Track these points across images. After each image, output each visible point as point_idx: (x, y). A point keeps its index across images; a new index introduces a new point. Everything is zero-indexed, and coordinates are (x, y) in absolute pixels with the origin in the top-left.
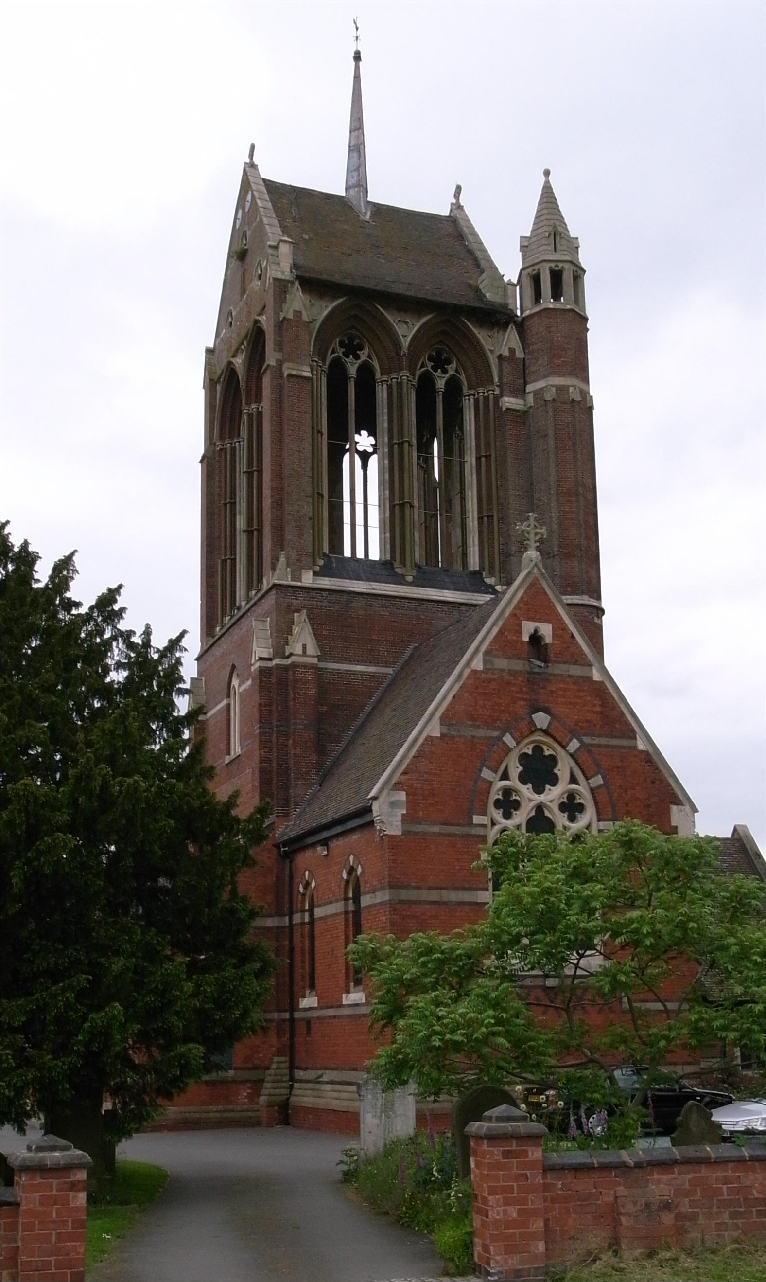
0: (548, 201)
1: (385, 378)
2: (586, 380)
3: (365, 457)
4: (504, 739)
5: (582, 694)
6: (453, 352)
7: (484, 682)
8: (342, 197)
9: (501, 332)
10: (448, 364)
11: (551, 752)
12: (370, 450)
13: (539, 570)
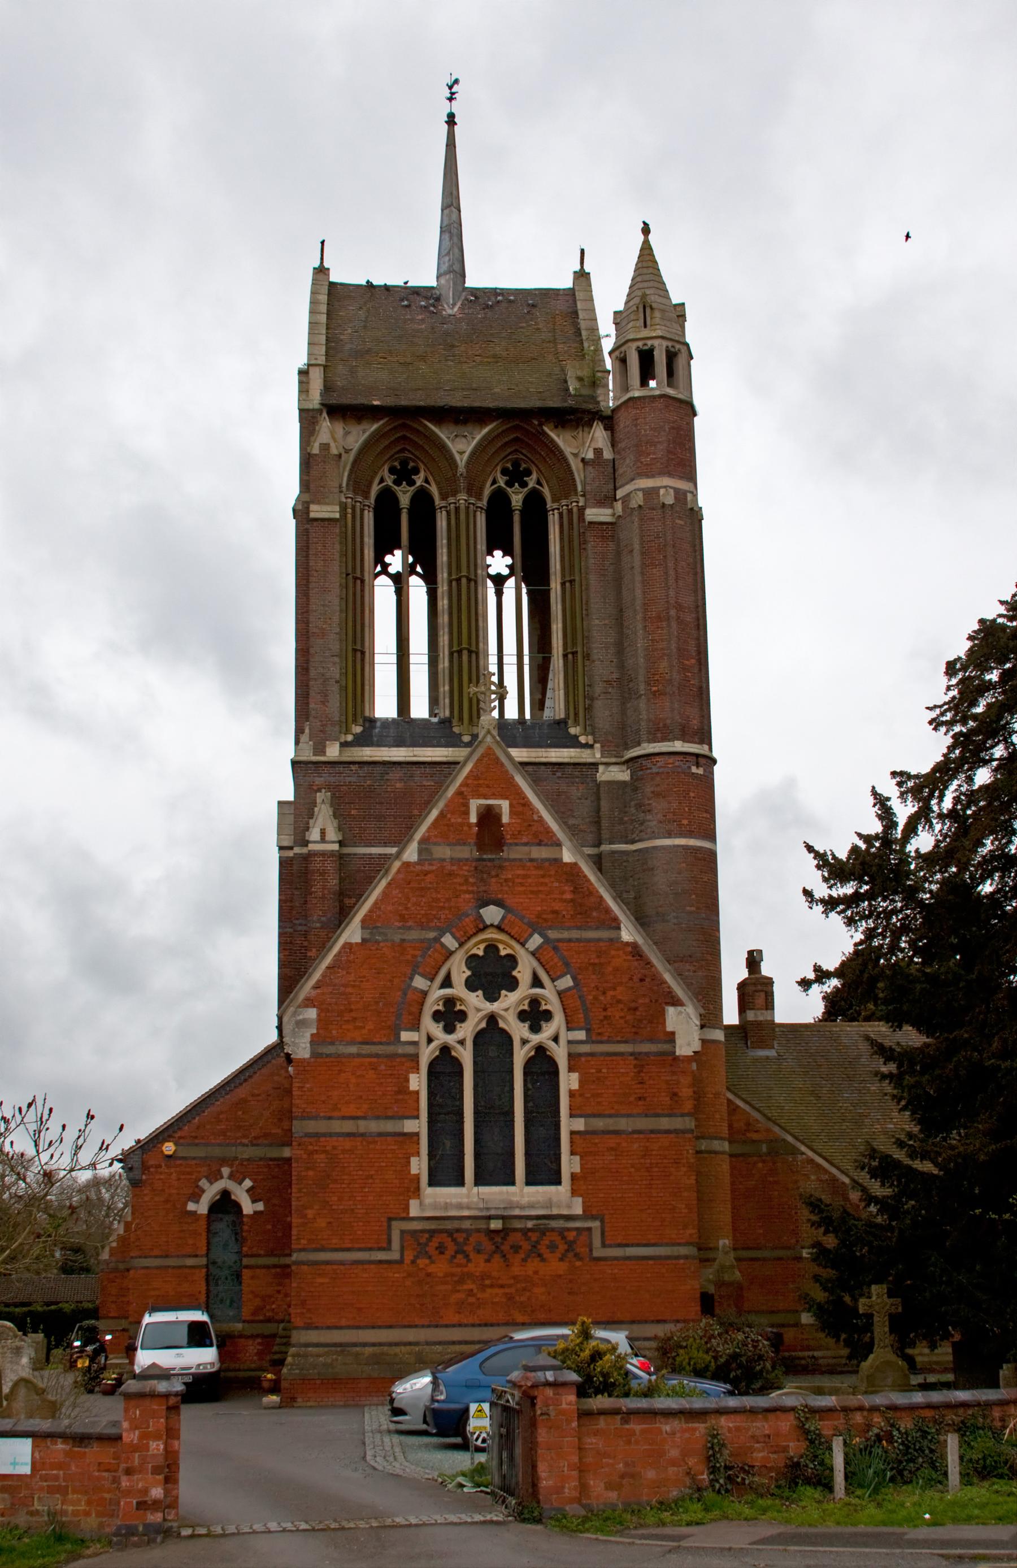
2: (691, 476)
3: (499, 581)
4: (443, 940)
5: (546, 880)
6: (533, 462)
7: (418, 875)
8: (433, 288)
9: (586, 429)
11: (509, 951)
12: (506, 572)
13: (494, 737)
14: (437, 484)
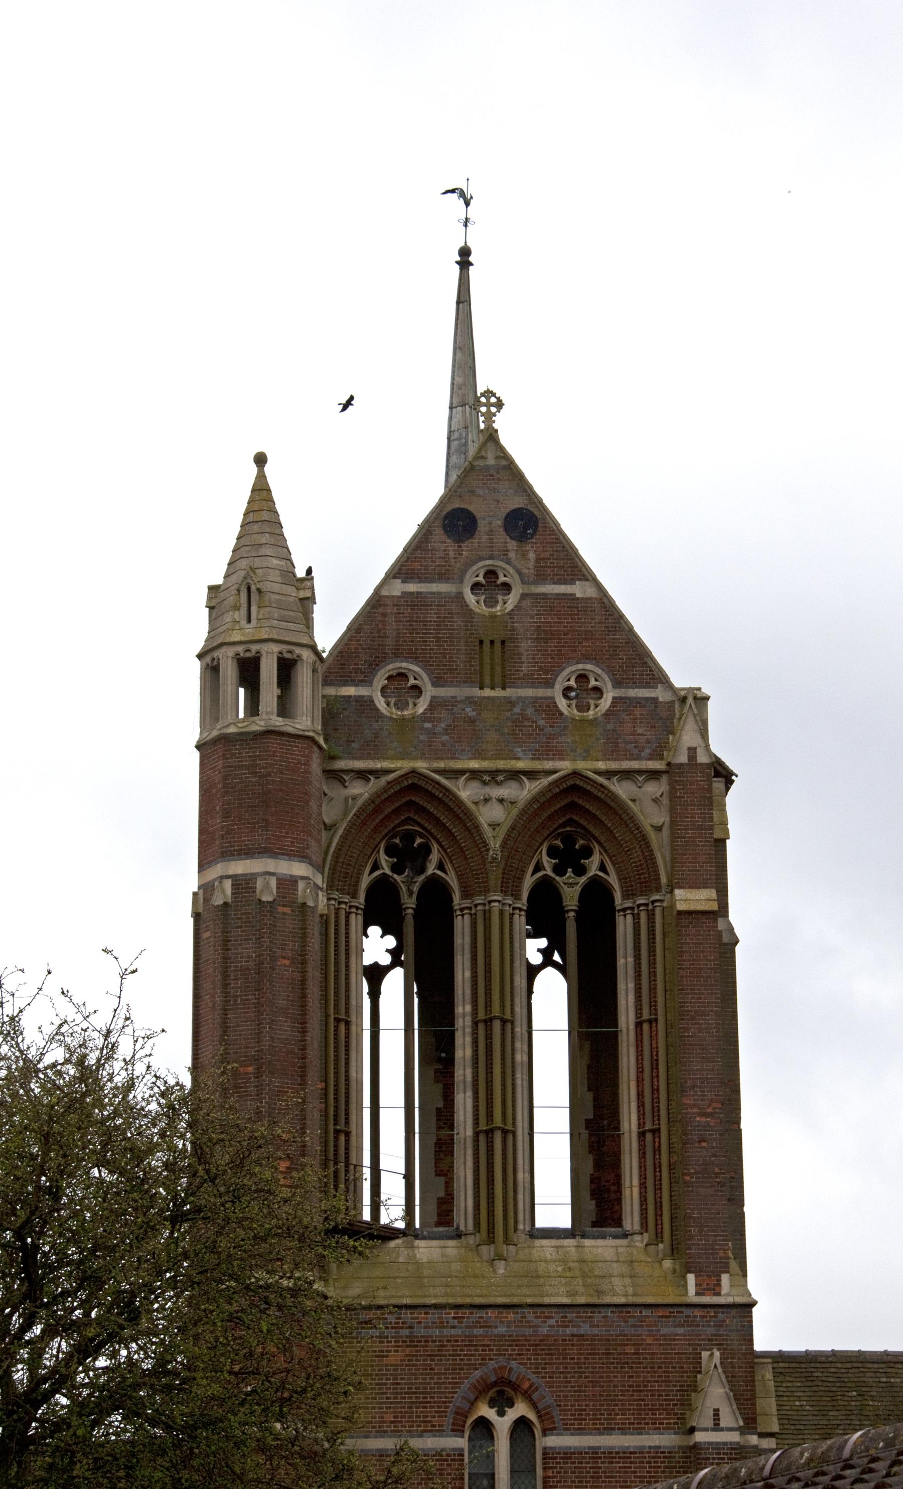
0: (261, 515)
1: (466, 903)
10: (588, 857)
14: (619, 872)
